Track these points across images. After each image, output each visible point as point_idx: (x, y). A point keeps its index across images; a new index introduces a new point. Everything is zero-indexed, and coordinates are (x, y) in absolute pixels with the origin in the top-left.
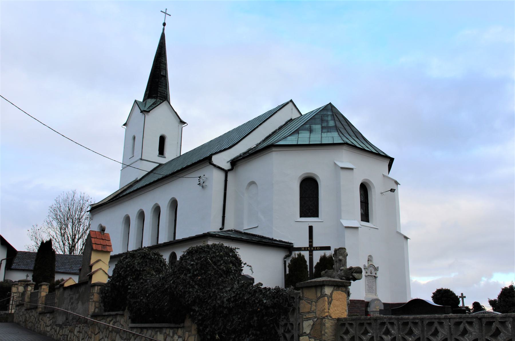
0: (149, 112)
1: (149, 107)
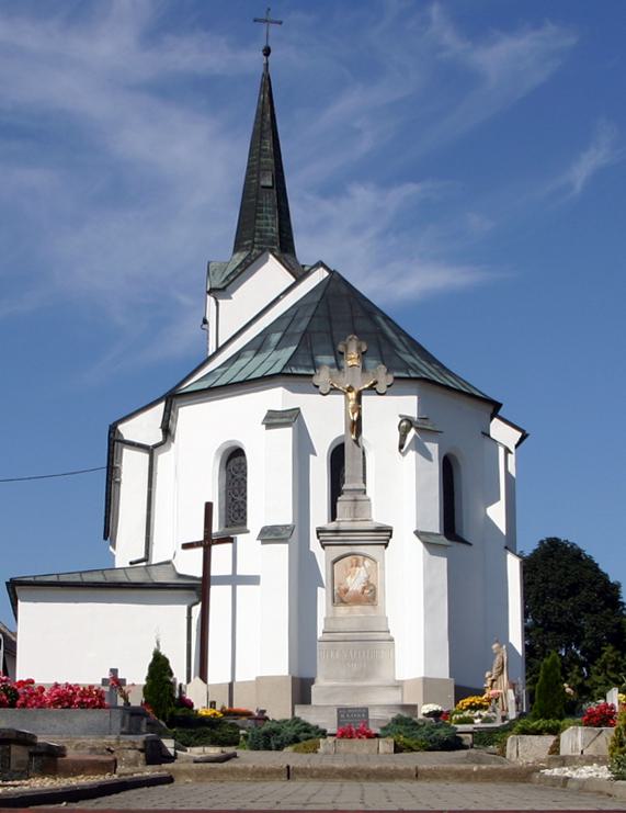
0: (224, 289)
1: (227, 278)
